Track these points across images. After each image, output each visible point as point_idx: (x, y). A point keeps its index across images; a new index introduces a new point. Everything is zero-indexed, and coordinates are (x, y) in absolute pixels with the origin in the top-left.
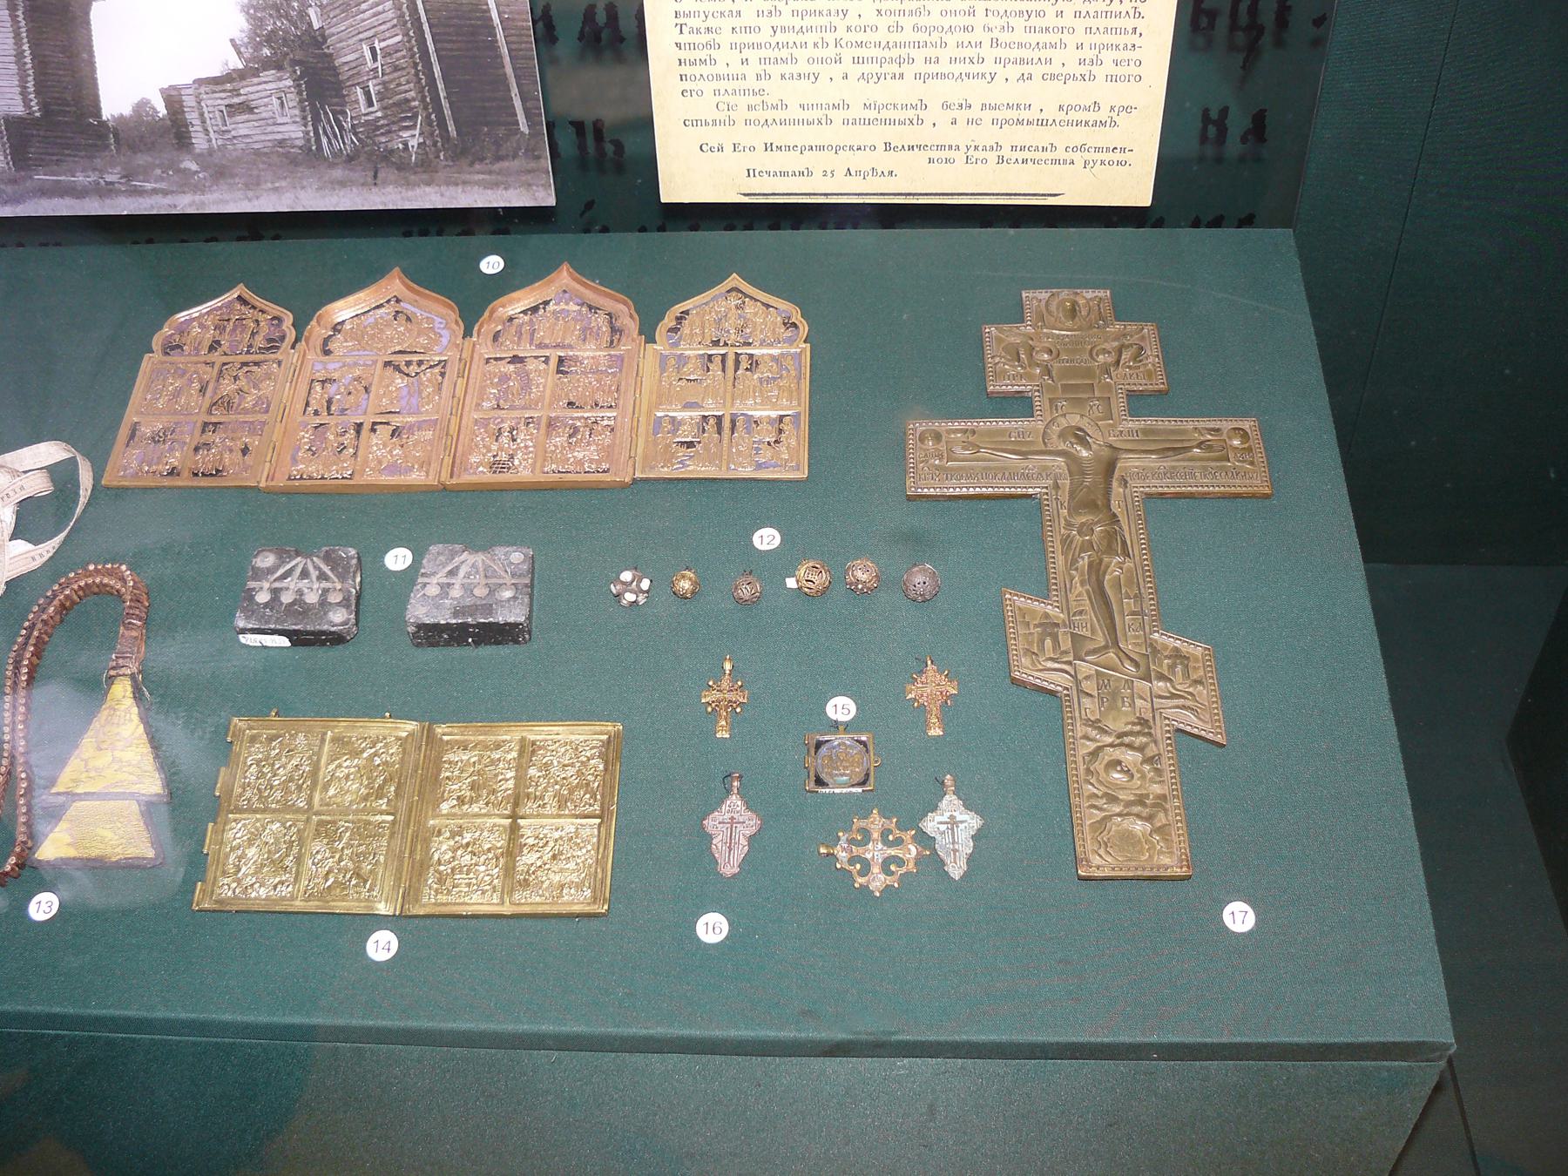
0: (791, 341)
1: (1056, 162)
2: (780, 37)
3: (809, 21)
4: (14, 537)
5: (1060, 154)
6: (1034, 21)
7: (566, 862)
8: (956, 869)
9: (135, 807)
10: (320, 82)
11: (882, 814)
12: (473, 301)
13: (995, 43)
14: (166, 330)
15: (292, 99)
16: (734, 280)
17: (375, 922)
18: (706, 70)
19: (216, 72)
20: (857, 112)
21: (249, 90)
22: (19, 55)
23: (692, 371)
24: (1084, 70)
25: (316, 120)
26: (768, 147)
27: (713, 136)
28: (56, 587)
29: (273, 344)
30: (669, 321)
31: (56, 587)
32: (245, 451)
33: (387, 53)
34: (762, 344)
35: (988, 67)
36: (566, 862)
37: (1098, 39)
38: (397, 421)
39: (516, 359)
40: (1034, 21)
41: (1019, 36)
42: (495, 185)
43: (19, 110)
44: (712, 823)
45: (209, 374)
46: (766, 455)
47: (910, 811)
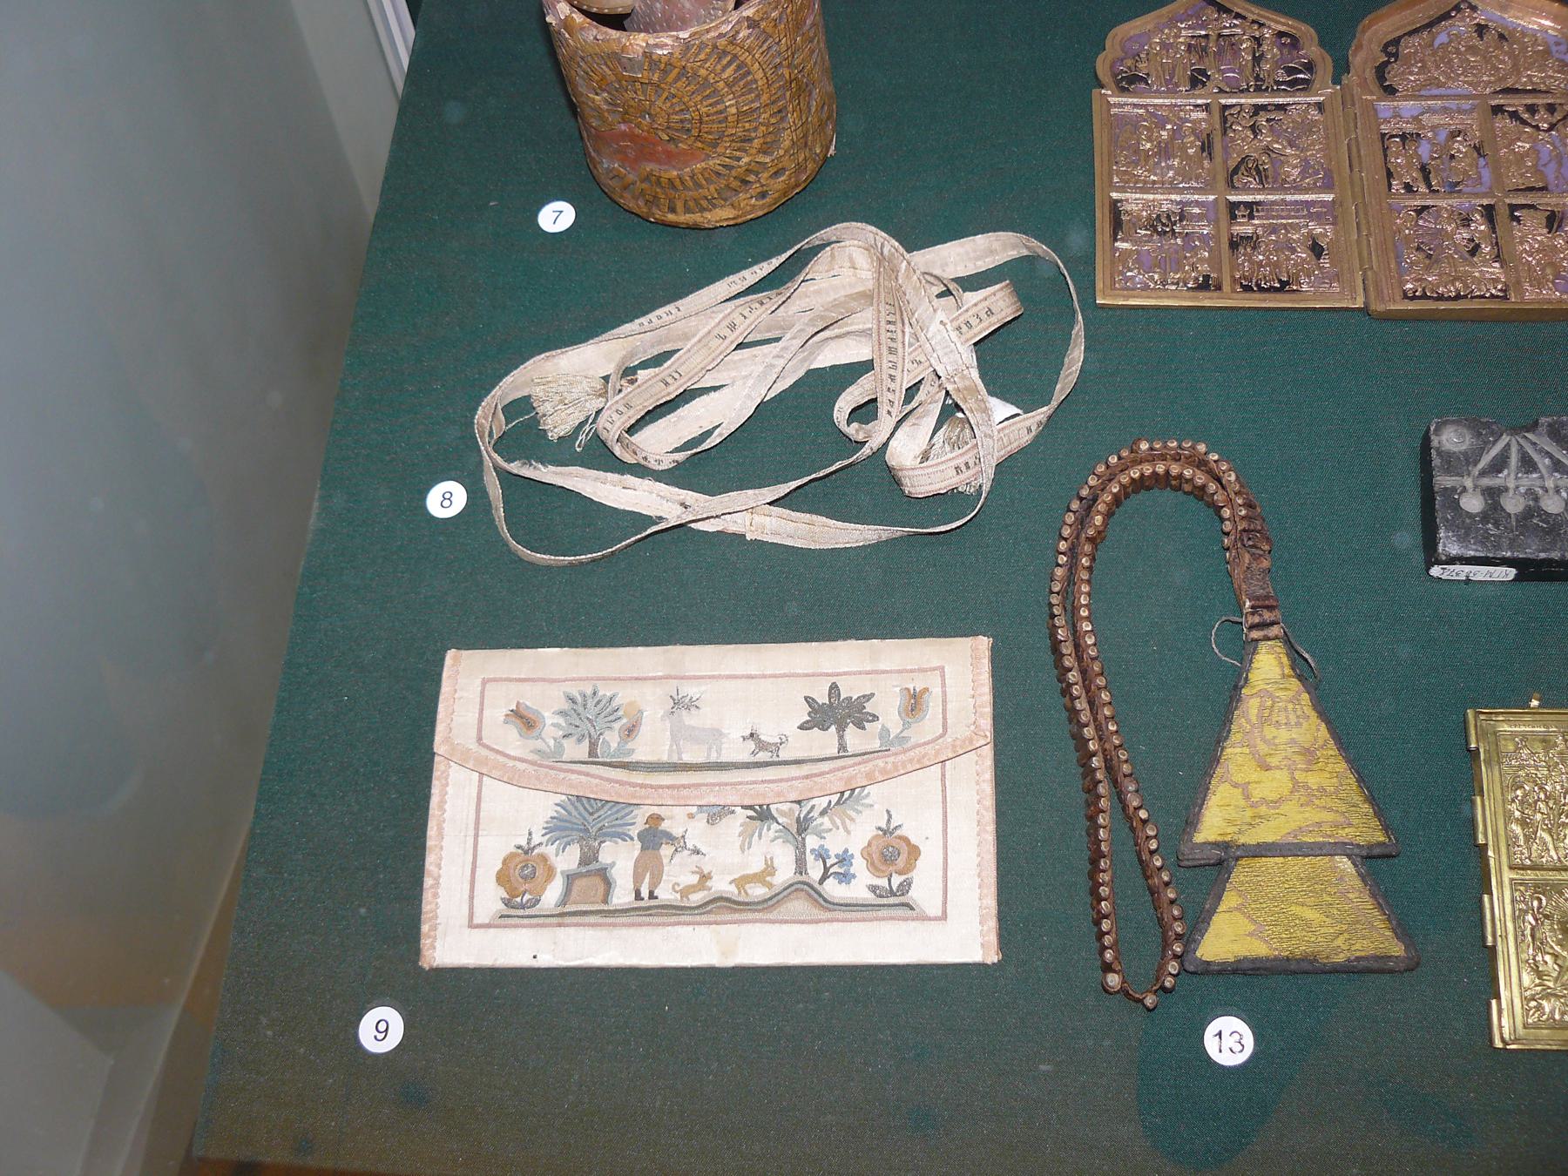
28: (1092, 481)
31: (1113, 460)
38: (1548, 201)
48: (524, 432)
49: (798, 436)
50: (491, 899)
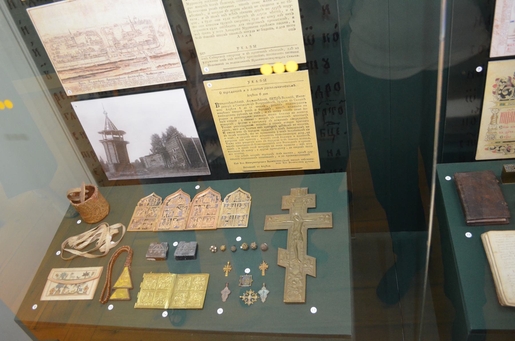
0: (248, 200)
1: (300, 162)
2: (244, 144)
3: (249, 141)
4: (111, 241)
5: (300, 161)
6: (290, 138)
7: (196, 300)
8: (263, 300)
9: (127, 290)
10: (166, 156)
11: (252, 290)
12: (193, 194)
13: (283, 142)
14: (140, 202)
15: (162, 159)
16: (239, 189)
17: (164, 310)
18: (232, 150)
19: (148, 155)
20: (261, 156)
21: (154, 157)
22: (115, 153)
23: (230, 207)
24: (300, 146)
25: (166, 162)
26: (246, 163)
27: (236, 161)
29: (158, 204)
30: (227, 197)
32: (151, 224)
33: (177, 150)
34: (243, 201)
35: (283, 146)
36: (196, 300)
37: (302, 140)
38: (178, 218)
39: (200, 206)
40: (290, 138)
41: (287, 141)
42: (199, 172)
43: (116, 162)
44: (222, 292)
45: (147, 210)
46: (241, 222)
47: (256, 290)
48: (67, 246)
49: (92, 247)
50: (49, 293)
